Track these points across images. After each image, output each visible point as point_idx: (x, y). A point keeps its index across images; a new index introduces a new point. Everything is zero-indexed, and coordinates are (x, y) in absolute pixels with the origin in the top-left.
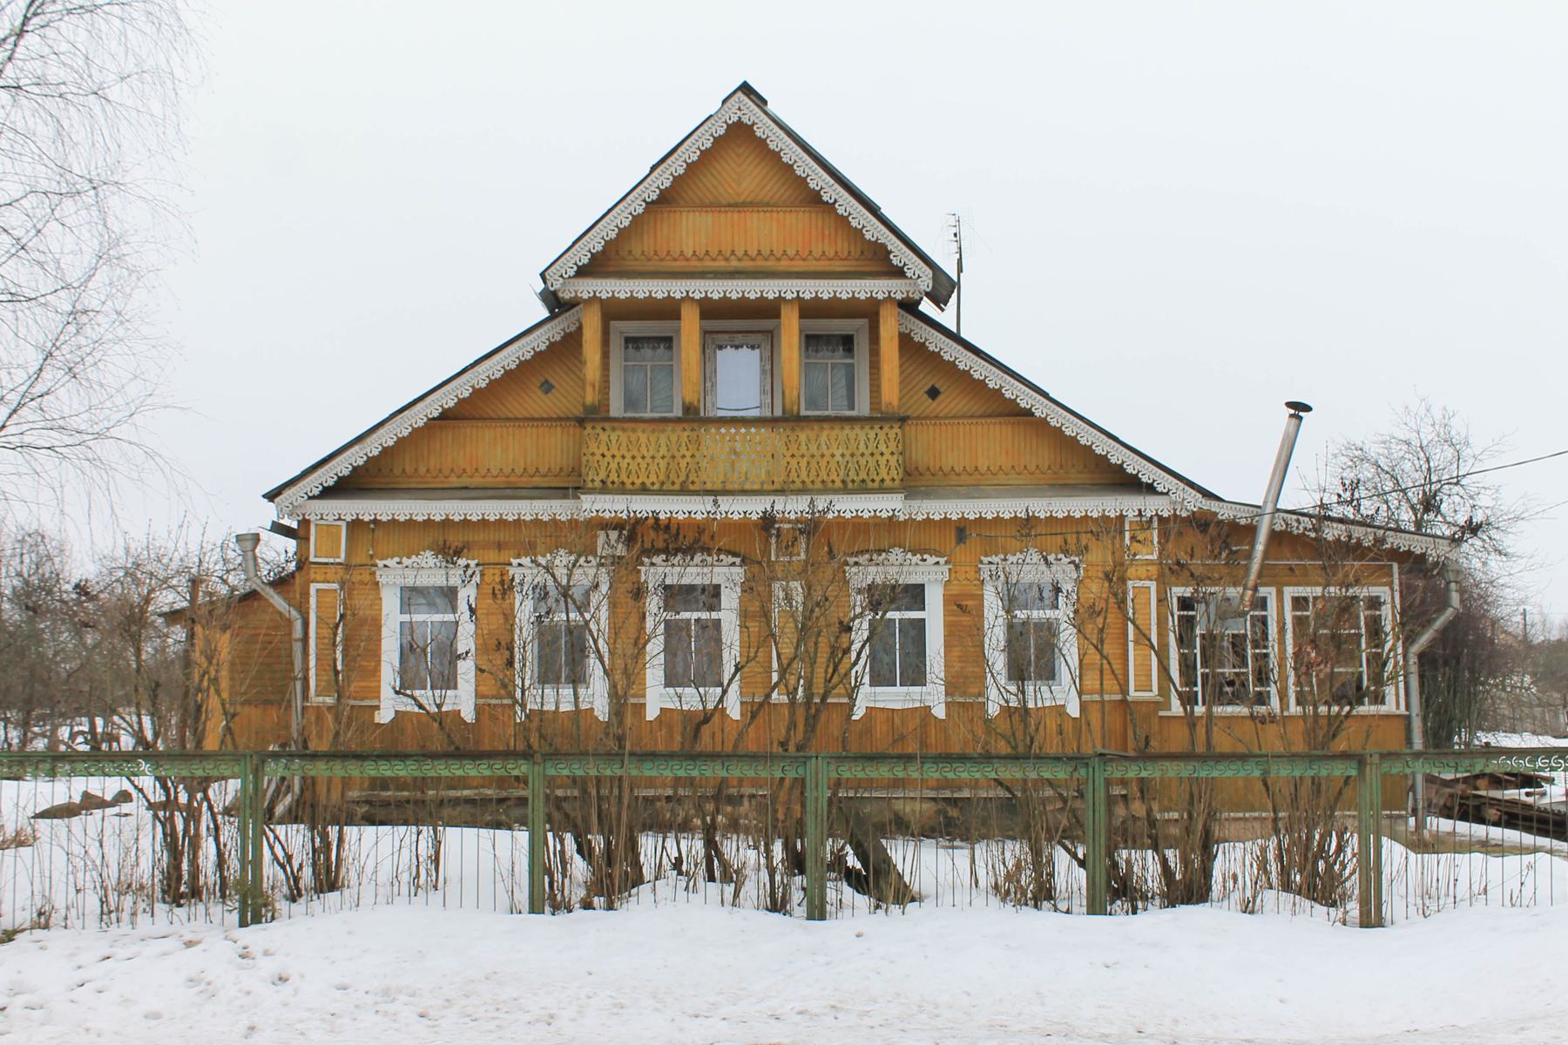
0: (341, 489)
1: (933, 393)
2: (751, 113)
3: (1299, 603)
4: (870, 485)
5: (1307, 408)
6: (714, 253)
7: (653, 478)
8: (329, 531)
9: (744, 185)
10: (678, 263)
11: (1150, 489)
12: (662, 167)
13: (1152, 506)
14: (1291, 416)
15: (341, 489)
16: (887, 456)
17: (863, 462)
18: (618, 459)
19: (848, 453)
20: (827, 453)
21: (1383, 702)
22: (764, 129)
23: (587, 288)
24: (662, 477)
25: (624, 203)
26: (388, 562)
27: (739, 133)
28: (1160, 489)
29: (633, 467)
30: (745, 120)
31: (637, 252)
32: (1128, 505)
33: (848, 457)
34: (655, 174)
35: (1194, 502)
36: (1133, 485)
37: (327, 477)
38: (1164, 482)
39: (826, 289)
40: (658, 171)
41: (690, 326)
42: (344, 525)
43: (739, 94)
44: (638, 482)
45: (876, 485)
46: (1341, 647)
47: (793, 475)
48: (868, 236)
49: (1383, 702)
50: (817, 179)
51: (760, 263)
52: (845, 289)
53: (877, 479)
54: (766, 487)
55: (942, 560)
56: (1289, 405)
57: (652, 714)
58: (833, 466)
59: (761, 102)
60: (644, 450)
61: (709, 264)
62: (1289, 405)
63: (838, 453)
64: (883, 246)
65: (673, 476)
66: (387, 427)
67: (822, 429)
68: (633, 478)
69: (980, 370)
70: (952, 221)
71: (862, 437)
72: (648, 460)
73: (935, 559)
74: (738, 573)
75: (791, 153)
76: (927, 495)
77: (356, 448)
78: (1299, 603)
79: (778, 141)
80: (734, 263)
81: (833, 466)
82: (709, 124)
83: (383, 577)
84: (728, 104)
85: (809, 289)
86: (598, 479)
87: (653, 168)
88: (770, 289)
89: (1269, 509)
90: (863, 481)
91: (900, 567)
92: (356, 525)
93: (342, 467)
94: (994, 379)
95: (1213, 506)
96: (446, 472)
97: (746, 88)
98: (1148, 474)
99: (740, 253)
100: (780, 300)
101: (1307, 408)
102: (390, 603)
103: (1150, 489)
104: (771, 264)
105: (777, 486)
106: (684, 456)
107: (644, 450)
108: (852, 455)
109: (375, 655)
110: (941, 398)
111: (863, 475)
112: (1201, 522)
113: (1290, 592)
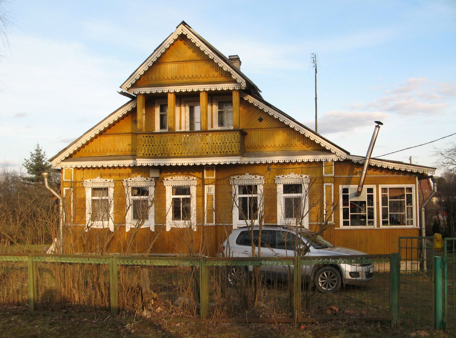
0: (69, 158)
1: (261, 120)
2: (186, 31)
3: (384, 190)
4: (229, 153)
5: (382, 124)
6: (178, 77)
7: (159, 152)
8: (68, 171)
9: (188, 54)
10: (179, 80)
11: (329, 152)
12: (157, 50)
13: (330, 157)
14: (376, 126)
15: (69, 158)
16: (235, 143)
17: (227, 145)
18: (148, 146)
19: (221, 142)
20: (215, 143)
21: (383, 225)
22: (190, 36)
23: (137, 91)
24: (161, 152)
25: (146, 63)
26: (279, 176)
27: (183, 37)
28: (333, 152)
29: (153, 149)
30: (184, 33)
31: (154, 78)
32: (321, 157)
33: (222, 144)
34: (155, 53)
35: (344, 156)
36: (324, 150)
37: (66, 154)
38: (334, 149)
39: (213, 87)
40: (156, 52)
41: (203, 98)
42: (73, 169)
43: (182, 25)
44: (154, 154)
45: (231, 153)
46: (397, 206)
47: (204, 150)
48: (224, 69)
49: (383, 225)
50: (208, 51)
51: (193, 80)
52: (219, 87)
53: (231, 151)
54: (195, 155)
55: (262, 177)
56: (376, 122)
57: (168, 229)
58: (217, 147)
59: (189, 27)
60: (156, 143)
61: (177, 81)
62: (376, 122)
63: (218, 142)
64: (230, 72)
65: (165, 151)
66: (83, 138)
67: (213, 135)
68: (153, 152)
69: (272, 112)
70: (313, 56)
71: (227, 137)
72: (157, 146)
73: (260, 177)
74: (195, 183)
75: (199, 44)
76: (249, 156)
77: (74, 145)
78: (384, 190)
79: (194, 40)
80: (185, 80)
81: (217, 147)
82: (172, 35)
83: (165, 183)
84: (178, 28)
85: (208, 87)
86: (142, 153)
87: (155, 51)
88: (195, 88)
89: (368, 158)
90: (227, 152)
91: (247, 179)
92: (76, 168)
93: (71, 151)
94: (276, 115)
95: (350, 158)
96: (105, 151)
97: (184, 23)
98: (329, 147)
99: (186, 77)
100: (199, 92)
101: (382, 124)
102: (89, 194)
103: (329, 152)
104: (196, 80)
105: (199, 154)
106: (162, 145)
107: (156, 143)
108: (223, 143)
109: (84, 209)
110: (263, 122)
111: (156, 153)
112: (347, 161)
113: (381, 186)
